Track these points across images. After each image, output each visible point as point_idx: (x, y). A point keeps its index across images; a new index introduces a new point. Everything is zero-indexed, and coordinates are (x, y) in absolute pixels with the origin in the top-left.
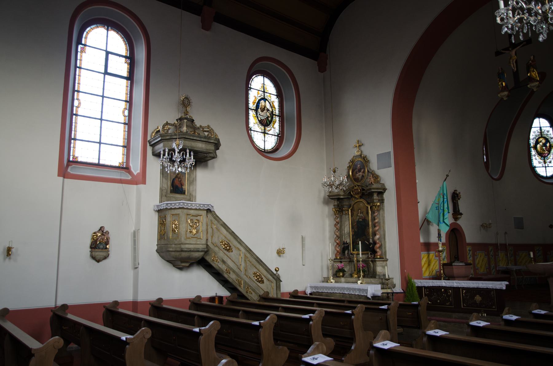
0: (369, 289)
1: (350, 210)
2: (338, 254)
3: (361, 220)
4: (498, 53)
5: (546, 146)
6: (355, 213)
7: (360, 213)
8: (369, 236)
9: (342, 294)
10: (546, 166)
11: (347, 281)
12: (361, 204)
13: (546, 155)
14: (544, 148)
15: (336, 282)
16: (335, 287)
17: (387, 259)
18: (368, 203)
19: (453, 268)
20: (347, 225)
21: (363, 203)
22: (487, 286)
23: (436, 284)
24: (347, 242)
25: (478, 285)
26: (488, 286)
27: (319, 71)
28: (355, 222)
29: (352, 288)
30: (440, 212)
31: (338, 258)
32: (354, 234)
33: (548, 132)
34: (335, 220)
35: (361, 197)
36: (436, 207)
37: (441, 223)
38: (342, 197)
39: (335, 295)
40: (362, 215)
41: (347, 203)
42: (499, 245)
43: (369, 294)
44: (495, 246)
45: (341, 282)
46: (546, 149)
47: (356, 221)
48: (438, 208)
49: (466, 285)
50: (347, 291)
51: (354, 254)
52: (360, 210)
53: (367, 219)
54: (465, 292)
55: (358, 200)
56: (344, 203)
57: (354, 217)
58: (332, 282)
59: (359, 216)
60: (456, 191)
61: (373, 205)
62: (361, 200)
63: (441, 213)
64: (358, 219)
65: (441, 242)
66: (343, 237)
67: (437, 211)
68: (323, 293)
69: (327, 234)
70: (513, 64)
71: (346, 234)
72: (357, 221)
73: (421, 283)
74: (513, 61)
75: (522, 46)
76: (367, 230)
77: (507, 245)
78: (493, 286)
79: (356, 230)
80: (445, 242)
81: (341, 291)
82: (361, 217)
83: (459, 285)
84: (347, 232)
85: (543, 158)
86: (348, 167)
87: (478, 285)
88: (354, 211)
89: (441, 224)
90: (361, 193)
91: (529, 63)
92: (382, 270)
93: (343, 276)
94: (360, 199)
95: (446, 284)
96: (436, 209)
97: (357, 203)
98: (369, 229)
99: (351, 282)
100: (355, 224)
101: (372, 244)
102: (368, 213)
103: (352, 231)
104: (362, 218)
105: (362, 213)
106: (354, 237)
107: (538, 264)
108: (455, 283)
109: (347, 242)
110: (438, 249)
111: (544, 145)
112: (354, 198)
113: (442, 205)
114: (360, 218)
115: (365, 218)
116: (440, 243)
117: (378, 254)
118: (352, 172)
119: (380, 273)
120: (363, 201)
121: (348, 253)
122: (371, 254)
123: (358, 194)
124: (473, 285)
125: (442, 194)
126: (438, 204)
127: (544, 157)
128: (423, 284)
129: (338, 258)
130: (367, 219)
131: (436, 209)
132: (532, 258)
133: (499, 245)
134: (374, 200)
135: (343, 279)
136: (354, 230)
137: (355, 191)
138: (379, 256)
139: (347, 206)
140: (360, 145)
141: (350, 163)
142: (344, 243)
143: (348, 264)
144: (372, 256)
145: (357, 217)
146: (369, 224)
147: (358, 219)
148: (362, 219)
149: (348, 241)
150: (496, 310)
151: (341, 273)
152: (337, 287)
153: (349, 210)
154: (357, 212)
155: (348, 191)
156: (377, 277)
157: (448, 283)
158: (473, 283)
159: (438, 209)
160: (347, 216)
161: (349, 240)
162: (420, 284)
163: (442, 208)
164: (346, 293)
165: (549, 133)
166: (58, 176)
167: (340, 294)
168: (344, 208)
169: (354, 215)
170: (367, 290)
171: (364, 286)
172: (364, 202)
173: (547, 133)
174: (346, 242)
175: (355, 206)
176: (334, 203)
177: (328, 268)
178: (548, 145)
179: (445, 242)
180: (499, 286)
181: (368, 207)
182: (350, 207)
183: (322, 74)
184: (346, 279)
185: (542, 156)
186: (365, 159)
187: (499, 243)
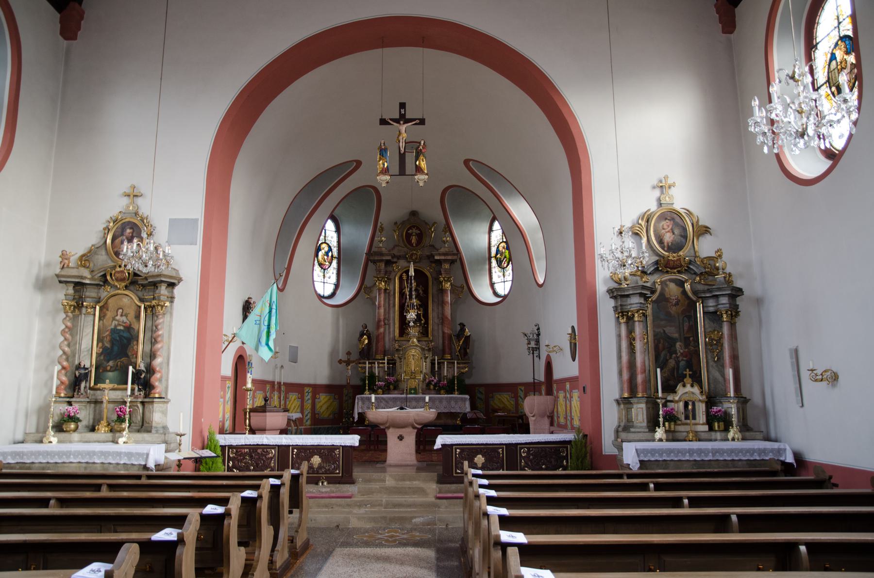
0: (151, 453)
1: (98, 308)
2: (62, 387)
3: (121, 328)
4: (383, 122)
5: (328, 256)
6: (109, 314)
7: (122, 315)
8: (136, 357)
9: (84, 465)
10: (325, 281)
11: (84, 440)
12: (126, 300)
13: (327, 268)
14: (326, 257)
15: (59, 442)
16: (71, 451)
17: (168, 399)
18: (142, 300)
19: (266, 416)
20: (87, 334)
21: (130, 299)
22: (332, 442)
23: (252, 441)
24: (86, 367)
25: (319, 441)
26: (334, 441)
27: (62, 34)
28: (107, 331)
29: (113, 452)
30: (262, 329)
31: (62, 395)
32: (102, 353)
33: (332, 237)
34: (64, 323)
35: (126, 287)
36: (255, 321)
37: (262, 346)
38: (87, 281)
39: (67, 467)
40: (124, 319)
41: (94, 294)
42: (276, 384)
43: (152, 461)
44: (272, 383)
45: (71, 442)
46: (327, 259)
47: (110, 328)
48: (258, 322)
49: (301, 441)
50: (99, 458)
51: (105, 388)
52: (120, 311)
53: (136, 328)
54: (296, 453)
55: (120, 292)
56: (87, 294)
57: (104, 320)
58: (51, 442)
59: (117, 320)
60: (250, 300)
61: (158, 305)
62: (127, 292)
63: (263, 331)
64: (116, 326)
65: (251, 376)
66: (77, 356)
67: (257, 327)
68: (34, 465)
69: (34, 348)
70: (402, 143)
71: (83, 352)
72: (112, 329)
73: (225, 440)
74: (403, 139)
75: (414, 124)
76: (133, 347)
77: (282, 384)
78: (341, 442)
79: (108, 345)
80: (231, 376)
81: (106, 460)
82: (121, 323)
83: (290, 441)
84: (86, 348)
85: (323, 270)
86: (104, 229)
87: (320, 440)
88: (107, 310)
89: (262, 348)
90: (128, 280)
91: (419, 149)
92: (161, 418)
93: (75, 430)
94: (124, 290)
95: (269, 441)
96: (255, 324)
97: (116, 297)
98: (137, 344)
99: (95, 442)
100: (108, 333)
101: (144, 371)
102: (138, 317)
103: (97, 347)
104: (124, 325)
105: (126, 316)
106: (102, 358)
107: (379, 411)
108: (284, 439)
109: (86, 367)
110: (245, 386)
111: (327, 254)
112: (109, 287)
113: (267, 318)
114: (119, 325)
115: (131, 325)
116: (250, 377)
117: (157, 391)
118: (113, 240)
119: (159, 424)
120: (131, 295)
121: (85, 387)
122: (139, 390)
123: (123, 280)
124: (326, 441)
125: (269, 302)
126: (260, 316)
127: (324, 270)
128: (229, 442)
129: (62, 395)
130: (134, 327)
131: (255, 324)
132: (373, 403)
133: (276, 384)
134: (161, 297)
135: (76, 436)
136: (103, 344)
137: (117, 275)
138: (158, 393)
139: (94, 299)
140: (133, 195)
141: (110, 222)
142: (78, 367)
143: (83, 408)
144: (140, 394)
145: (114, 322)
146: (138, 337)
147: (115, 325)
148: (124, 327)
149: (88, 365)
150: (341, 475)
151: (72, 423)
152: (74, 451)
153: (95, 308)
154: (115, 312)
155: (101, 272)
156: (153, 431)
157: (297, 439)
158: (313, 438)
159: (260, 324)
160: (91, 318)
161: (88, 361)
162: (224, 442)
163: (266, 323)
164: (96, 462)
165: (332, 240)
166: (424, 124)
167: (82, 464)
168: (85, 302)
169: (107, 317)
170: (148, 455)
171: (133, 448)
172: (134, 298)
173: (331, 239)
174: (85, 365)
175: (110, 301)
176: (67, 290)
177: (27, 416)
178: (330, 254)
179: (231, 376)
180: (349, 442)
181: (140, 307)
182: (98, 302)
183: (65, 41)
184: (83, 435)
185: (322, 268)
186: (145, 221)
187: (276, 381)
